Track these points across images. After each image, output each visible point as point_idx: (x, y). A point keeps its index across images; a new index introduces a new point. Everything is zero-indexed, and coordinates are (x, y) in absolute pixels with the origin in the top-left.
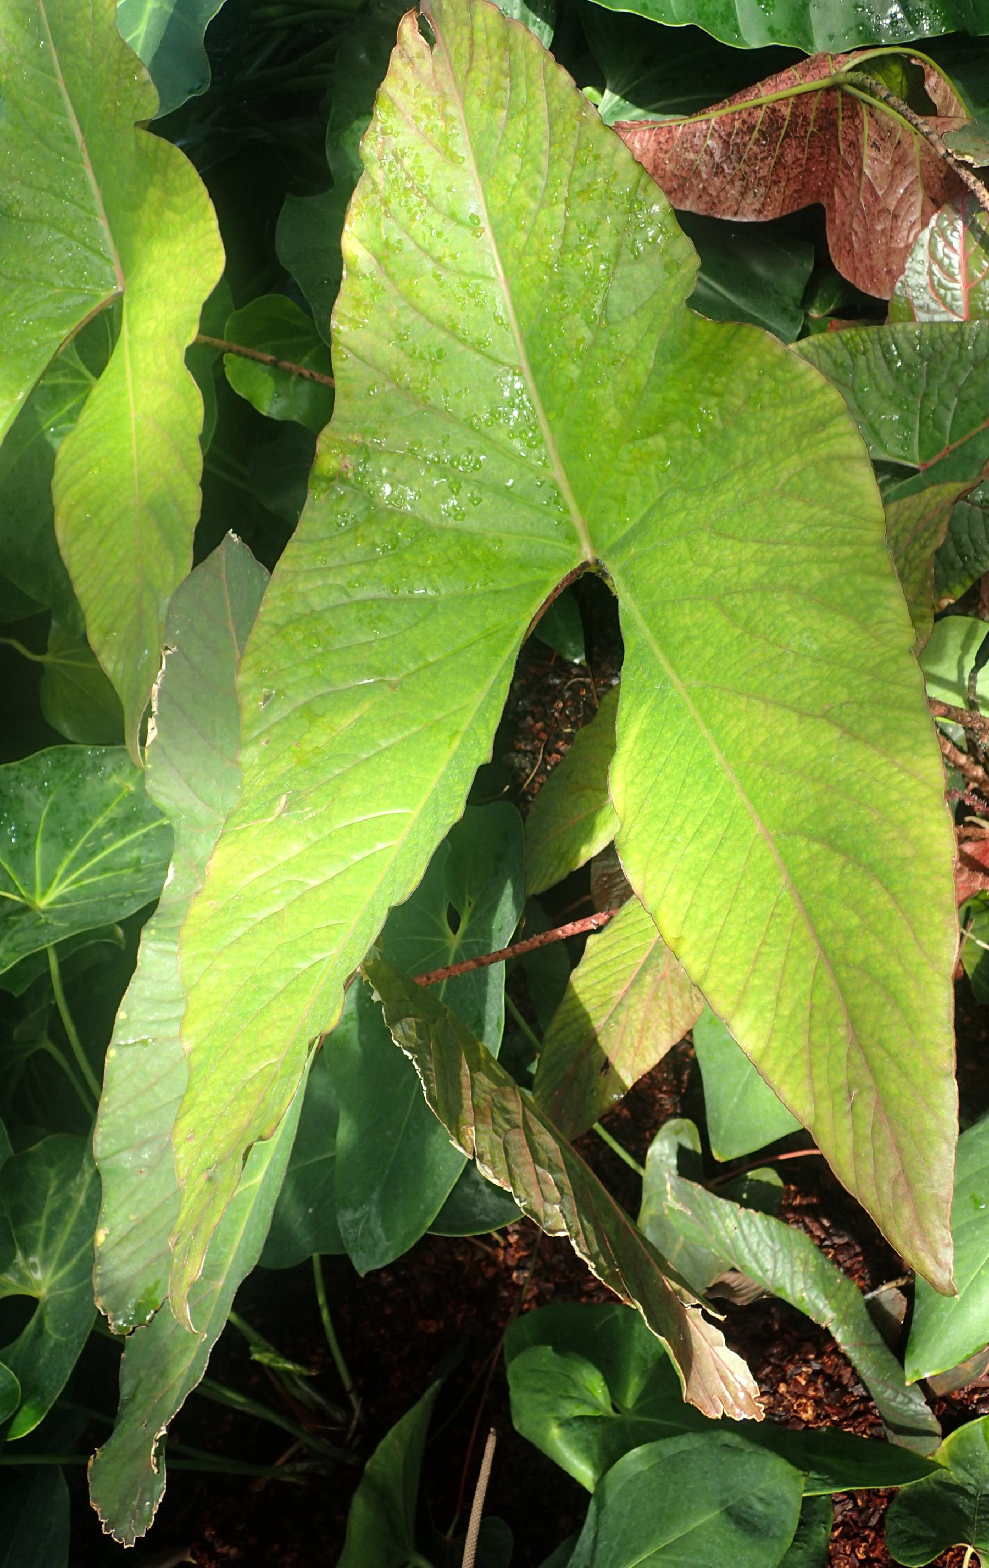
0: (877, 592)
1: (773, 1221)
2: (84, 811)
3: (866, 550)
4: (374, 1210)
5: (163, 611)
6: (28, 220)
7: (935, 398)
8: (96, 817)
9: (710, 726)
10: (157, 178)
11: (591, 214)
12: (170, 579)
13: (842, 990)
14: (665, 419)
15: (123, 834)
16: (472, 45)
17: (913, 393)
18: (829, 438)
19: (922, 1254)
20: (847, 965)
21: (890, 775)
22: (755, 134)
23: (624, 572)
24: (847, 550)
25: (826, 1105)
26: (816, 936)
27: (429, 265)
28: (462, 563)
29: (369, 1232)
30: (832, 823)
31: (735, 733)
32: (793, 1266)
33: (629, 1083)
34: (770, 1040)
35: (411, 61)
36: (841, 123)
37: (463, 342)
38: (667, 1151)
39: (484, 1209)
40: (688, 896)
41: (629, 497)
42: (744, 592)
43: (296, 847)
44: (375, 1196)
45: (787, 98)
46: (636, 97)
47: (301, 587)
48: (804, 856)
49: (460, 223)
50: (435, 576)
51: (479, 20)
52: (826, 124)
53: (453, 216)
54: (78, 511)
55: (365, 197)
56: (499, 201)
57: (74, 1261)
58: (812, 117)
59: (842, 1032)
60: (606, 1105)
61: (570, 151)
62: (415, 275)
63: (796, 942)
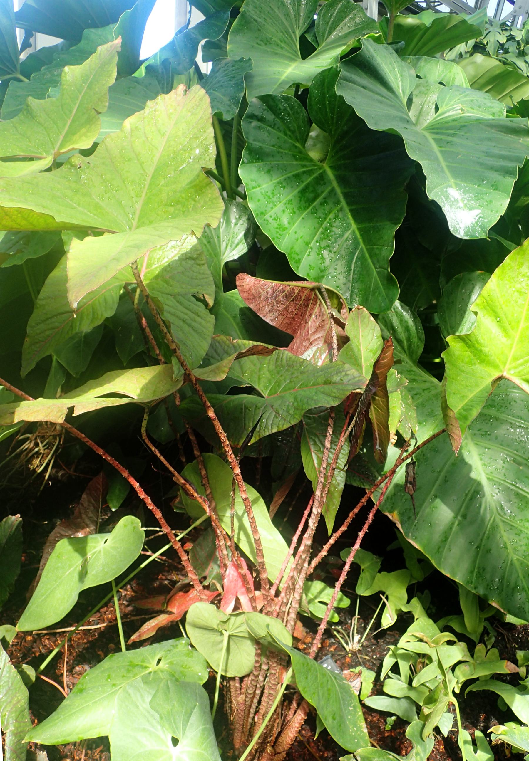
14: (178, 202)
22: (284, 294)
37: (138, 160)
58: (303, 297)
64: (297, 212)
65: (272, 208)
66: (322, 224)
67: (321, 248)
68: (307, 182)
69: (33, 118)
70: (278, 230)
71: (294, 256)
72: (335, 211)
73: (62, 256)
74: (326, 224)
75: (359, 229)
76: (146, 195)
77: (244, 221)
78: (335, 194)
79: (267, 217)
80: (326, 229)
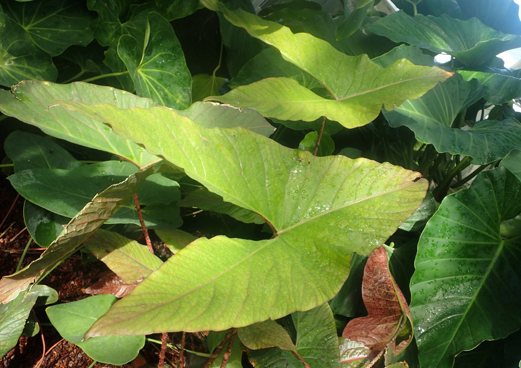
0: (283, 309)
1: (21, 332)
2: (170, 86)
3: (294, 305)
4: (34, 182)
5: (252, 108)
6: (354, 74)
7: (317, 352)
8: (168, 90)
9: (240, 264)
10: (369, 110)
11: (375, 225)
12: (261, 110)
13: (172, 302)
14: (321, 251)
15: (163, 98)
16: (415, 191)
17: (318, 345)
18: (321, 295)
19: (98, 327)
20: (180, 303)
21: (235, 313)
22: (387, 291)
23: (276, 241)
24: (293, 301)
25: (138, 298)
26: (187, 294)
27: (357, 182)
28: (276, 194)
29: (25, 180)
30: (219, 297)
31: (239, 271)
32: (3, 341)
33: (102, 260)
34: (155, 282)
35: (409, 175)
36: (392, 316)
37: (338, 192)
38: (45, 292)
39: (33, 222)
40: (192, 258)
41: (298, 242)
42: (277, 273)
43: (193, 144)
44: (39, 182)
45: (398, 299)
46: (393, 258)
47: (267, 147)
48: (209, 290)
49: (369, 190)
50: (272, 186)
51: (421, 193)
52: (392, 312)
53: (371, 188)
54: (277, 85)
55: (374, 164)
56: (376, 200)
57: (12, 77)
58: (393, 307)
59: (160, 302)
60: (94, 252)
61: (391, 219)
62: (355, 178)
63: (184, 289)
64: (452, 253)
65: (439, 237)
66: (457, 275)
67: (441, 287)
68: (479, 243)
69: (356, 67)
70: (428, 253)
71: (420, 275)
72: (474, 276)
73: (190, 232)
74: (460, 277)
75: (474, 303)
76: (315, 219)
77: (426, 215)
78: (487, 266)
79: (431, 239)
80: (457, 280)
